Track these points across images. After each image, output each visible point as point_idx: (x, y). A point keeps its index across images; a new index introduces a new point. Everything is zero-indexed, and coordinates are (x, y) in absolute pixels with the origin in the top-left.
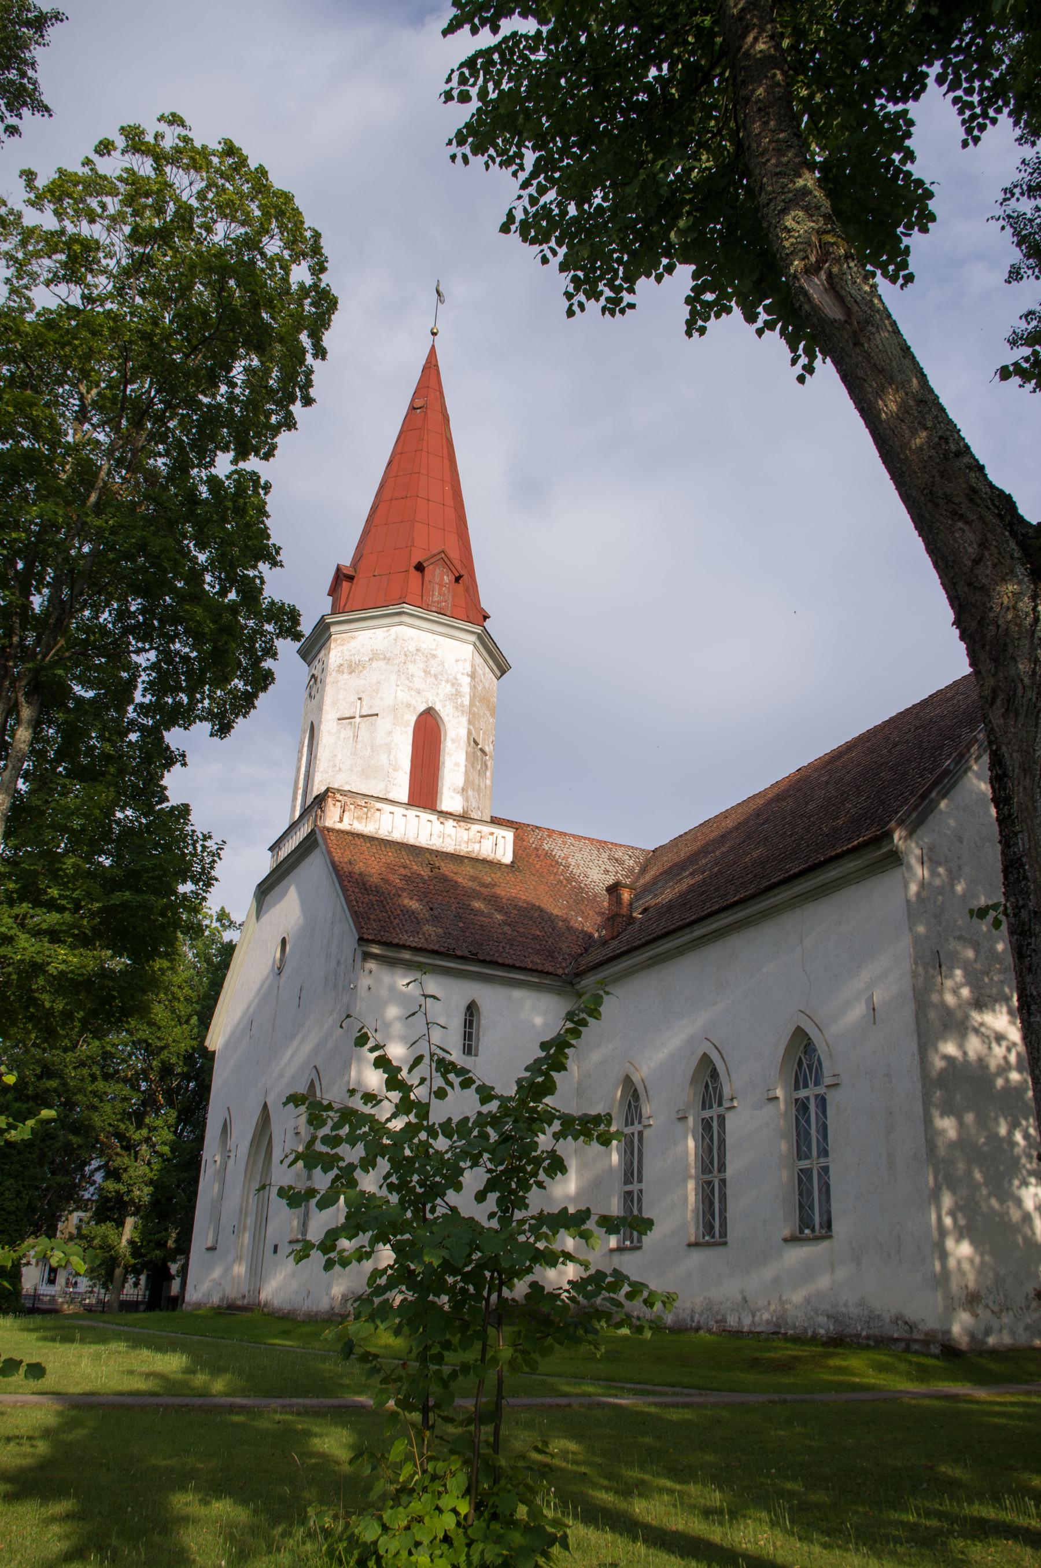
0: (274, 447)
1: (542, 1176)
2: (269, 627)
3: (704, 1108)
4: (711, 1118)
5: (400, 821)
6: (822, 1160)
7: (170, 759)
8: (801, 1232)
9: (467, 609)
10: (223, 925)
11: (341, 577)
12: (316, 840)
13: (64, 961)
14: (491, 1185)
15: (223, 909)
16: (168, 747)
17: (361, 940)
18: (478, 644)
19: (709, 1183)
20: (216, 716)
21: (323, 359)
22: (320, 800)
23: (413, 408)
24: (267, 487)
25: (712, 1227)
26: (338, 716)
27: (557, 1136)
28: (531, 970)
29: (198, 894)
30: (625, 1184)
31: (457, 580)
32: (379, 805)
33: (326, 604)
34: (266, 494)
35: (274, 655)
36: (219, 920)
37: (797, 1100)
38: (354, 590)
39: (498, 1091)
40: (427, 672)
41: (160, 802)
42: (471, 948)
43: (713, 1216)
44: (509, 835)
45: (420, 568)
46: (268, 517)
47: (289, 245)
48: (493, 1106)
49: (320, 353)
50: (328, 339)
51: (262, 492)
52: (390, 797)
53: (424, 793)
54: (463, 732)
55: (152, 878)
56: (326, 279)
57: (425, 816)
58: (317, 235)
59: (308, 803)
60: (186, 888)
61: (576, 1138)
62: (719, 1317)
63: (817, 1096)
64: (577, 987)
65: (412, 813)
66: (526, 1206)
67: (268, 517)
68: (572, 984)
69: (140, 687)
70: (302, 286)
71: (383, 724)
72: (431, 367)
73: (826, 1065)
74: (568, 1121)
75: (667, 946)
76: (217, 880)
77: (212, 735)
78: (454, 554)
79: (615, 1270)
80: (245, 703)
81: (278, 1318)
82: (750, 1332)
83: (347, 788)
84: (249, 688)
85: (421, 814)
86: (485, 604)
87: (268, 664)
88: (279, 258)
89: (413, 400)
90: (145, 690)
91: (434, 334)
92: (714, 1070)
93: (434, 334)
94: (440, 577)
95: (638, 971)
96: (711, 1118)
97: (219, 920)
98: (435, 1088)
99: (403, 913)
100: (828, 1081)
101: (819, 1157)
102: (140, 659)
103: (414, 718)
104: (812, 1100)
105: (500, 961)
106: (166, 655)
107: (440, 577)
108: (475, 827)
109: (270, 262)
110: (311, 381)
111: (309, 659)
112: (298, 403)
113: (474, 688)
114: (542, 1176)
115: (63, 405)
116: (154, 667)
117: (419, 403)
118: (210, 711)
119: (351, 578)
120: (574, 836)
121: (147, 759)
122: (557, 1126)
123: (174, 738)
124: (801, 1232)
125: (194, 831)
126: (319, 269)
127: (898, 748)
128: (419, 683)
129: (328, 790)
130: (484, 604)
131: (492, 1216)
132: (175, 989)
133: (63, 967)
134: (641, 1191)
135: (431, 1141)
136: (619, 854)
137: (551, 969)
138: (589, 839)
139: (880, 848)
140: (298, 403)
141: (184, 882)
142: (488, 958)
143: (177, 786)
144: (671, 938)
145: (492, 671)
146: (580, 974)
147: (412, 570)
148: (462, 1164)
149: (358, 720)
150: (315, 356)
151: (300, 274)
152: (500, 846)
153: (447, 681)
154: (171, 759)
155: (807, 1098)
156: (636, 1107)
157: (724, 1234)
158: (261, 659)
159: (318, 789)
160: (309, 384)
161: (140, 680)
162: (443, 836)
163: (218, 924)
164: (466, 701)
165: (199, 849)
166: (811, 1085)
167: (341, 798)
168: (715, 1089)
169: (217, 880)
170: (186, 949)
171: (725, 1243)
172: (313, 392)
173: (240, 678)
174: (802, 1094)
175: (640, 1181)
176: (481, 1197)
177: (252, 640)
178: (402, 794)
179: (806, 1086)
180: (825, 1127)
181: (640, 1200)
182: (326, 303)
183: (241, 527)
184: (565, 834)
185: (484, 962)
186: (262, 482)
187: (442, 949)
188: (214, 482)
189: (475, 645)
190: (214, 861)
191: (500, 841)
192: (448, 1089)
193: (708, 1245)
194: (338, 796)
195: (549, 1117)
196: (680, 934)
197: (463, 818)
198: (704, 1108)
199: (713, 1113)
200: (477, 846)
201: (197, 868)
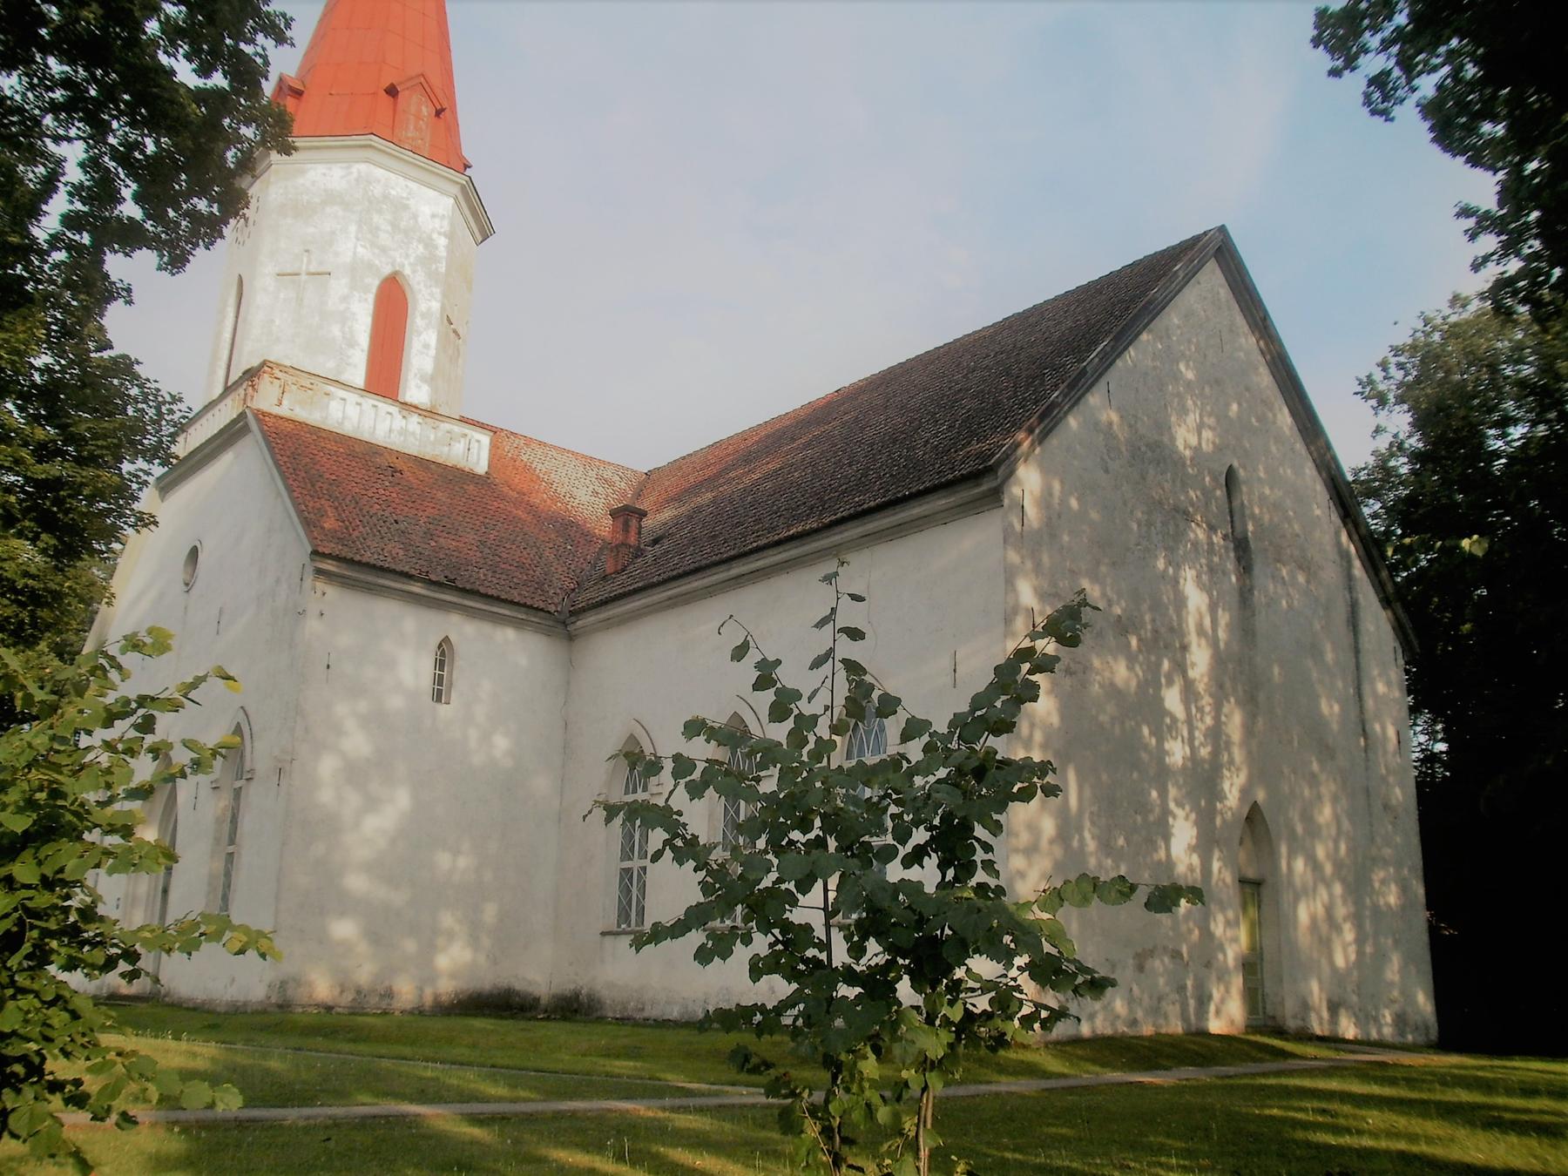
5: (352, 412)
9: (445, 152)
17: (315, 553)
18: (461, 198)
20: (165, 243)
22: (251, 375)
25: (628, 916)
26: (277, 270)
28: (518, 604)
29: (137, 477)
31: (438, 113)
40: (395, 226)
42: (447, 573)
44: (485, 439)
45: (392, 91)
52: (342, 379)
53: (384, 377)
54: (435, 306)
57: (385, 407)
59: (233, 378)
65: (369, 401)
68: (564, 624)
71: (338, 286)
75: (695, 584)
78: (435, 81)
80: (208, 229)
81: (188, 1009)
83: (288, 363)
85: (380, 405)
86: (468, 153)
95: (650, 613)
105: (482, 590)
107: (416, 106)
108: (446, 426)
113: (450, 250)
119: (298, 94)
120: (555, 447)
123: (116, 265)
125: (158, 390)
127: (978, 374)
128: (384, 239)
129: (264, 363)
136: (608, 474)
137: (542, 605)
139: (978, 485)
142: (468, 587)
143: (121, 328)
144: (699, 575)
146: (576, 613)
149: (304, 277)
152: (473, 453)
154: (111, 292)
167: (280, 375)
178: (358, 377)
185: (465, 592)
187: (413, 572)
189: (456, 199)
191: (474, 445)
194: (277, 372)
196: (714, 570)
197: (430, 413)
200: (446, 449)
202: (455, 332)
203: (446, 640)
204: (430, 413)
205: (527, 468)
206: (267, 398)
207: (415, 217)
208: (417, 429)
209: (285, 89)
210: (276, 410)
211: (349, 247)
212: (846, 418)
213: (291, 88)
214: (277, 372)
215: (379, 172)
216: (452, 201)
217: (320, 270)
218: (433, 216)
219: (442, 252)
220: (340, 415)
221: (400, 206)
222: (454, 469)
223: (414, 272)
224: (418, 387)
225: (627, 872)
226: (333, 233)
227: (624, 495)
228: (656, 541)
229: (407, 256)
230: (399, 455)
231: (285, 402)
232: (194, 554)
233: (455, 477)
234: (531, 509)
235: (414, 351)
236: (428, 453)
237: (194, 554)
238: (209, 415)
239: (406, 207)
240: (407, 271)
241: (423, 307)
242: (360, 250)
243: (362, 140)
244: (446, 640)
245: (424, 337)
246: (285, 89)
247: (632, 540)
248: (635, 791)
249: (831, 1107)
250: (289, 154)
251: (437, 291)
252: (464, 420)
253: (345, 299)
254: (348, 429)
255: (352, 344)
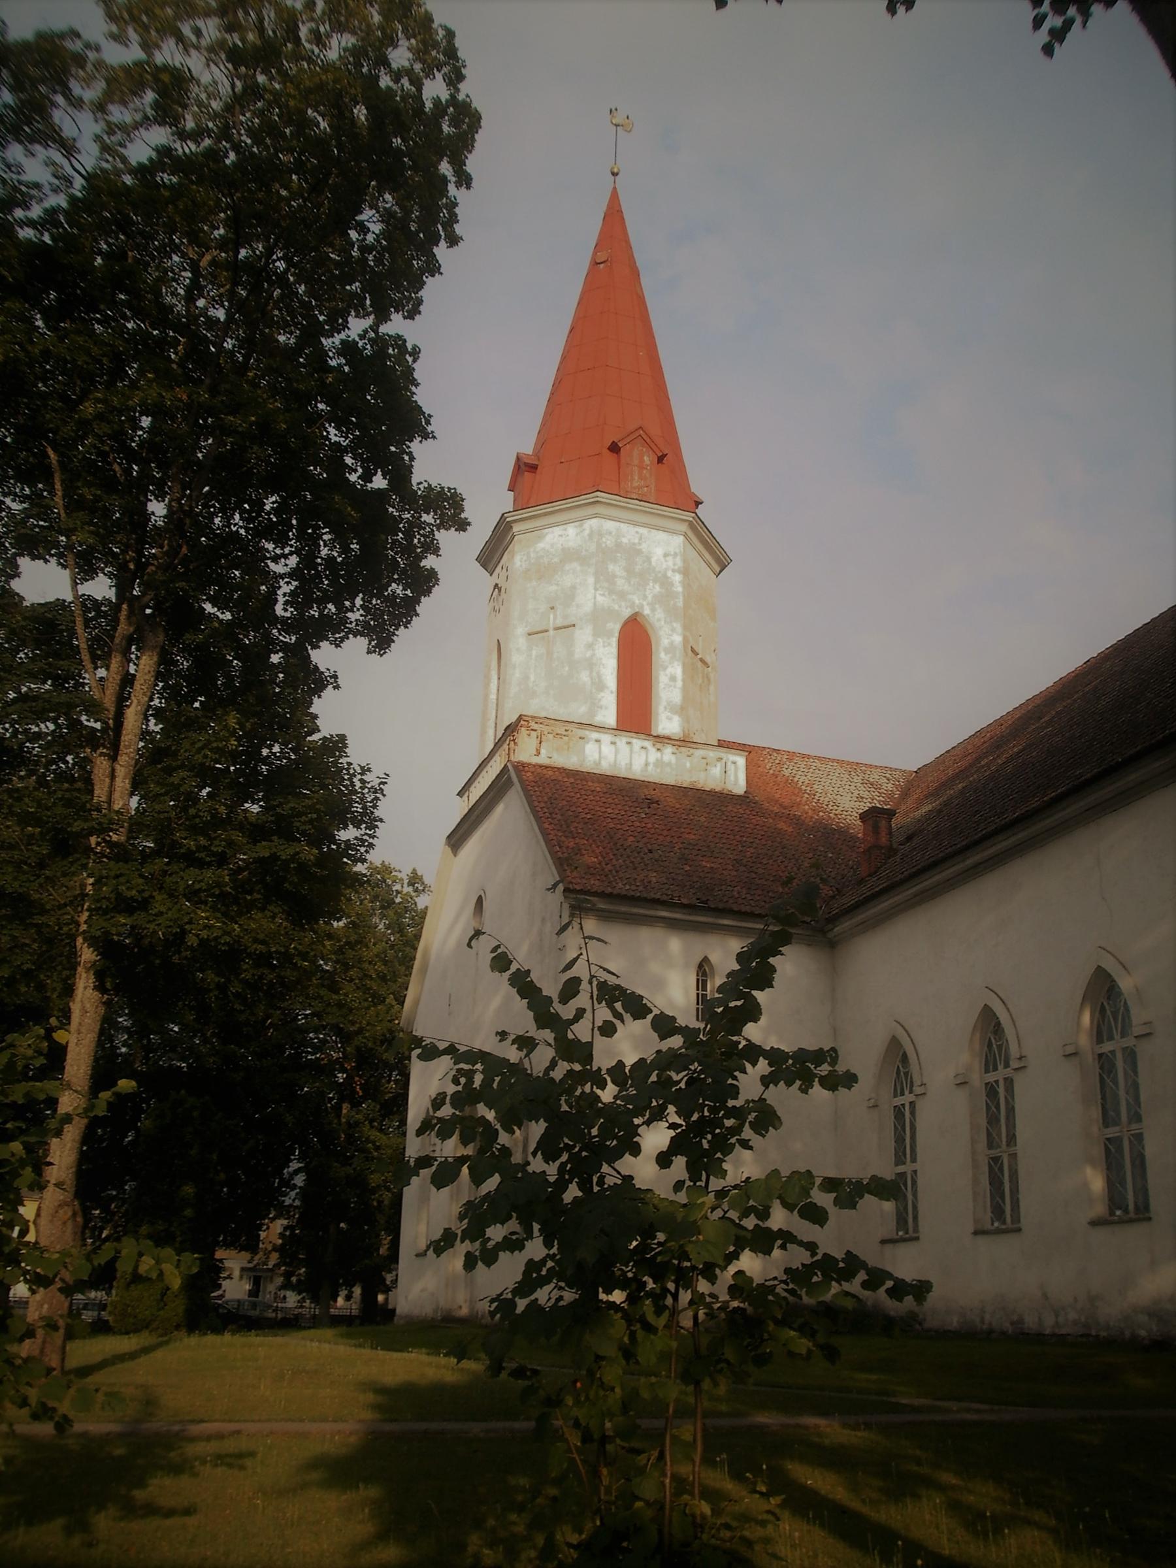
0: (420, 302)
1: (747, 1133)
2: (427, 518)
3: (987, 1071)
4: (997, 1082)
5: (607, 750)
6: (1134, 1126)
7: (319, 682)
8: (1112, 1213)
9: (673, 493)
10: (416, 890)
11: (524, 468)
12: (509, 778)
13: (206, 927)
14: (676, 1146)
15: (414, 872)
16: (316, 667)
18: (690, 534)
19: (996, 1160)
21: (468, 187)
23: (595, 263)
24: (416, 353)
25: (1003, 1212)
27: (766, 1081)
29: (363, 841)
30: (897, 1165)
31: (660, 460)
32: (581, 733)
33: (506, 501)
34: (414, 361)
35: (436, 551)
36: (411, 884)
37: (1100, 1056)
38: (536, 481)
39: (681, 1021)
40: (629, 571)
41: (311, 733)
43: (1003, 1197)
44: (741, 761)
45: (614, 448)
46: (417, 385)
47: (420, 54)
48: (676, 1041)
49: (465, 180)
50: (473, 163)
51: (410, 359)
53: (635, 715)
54: (678, 639)
55: (304, 823)
56: (465, 88)
57: (637, 743)
58: (450, 34)
60: (348, 834)
61: (789, 1084)
62: (1015, 1318)
63: (1124, 1049)
64: (830, 935)
65: (622, 740)
66: (724, 1173)
67: (417, 385)
68: (823, 932)
69: (281, 600)
70: (437, 102)
71: (583, 635)
72: (614, 216)
73: (1134, 1011)
74: (775, 1056)
76: (381, 820)
77: (369, 652)
79: (848, 1253)
80: (405, 611)
82: (1053, 1335)
83: (543, 714)
84: (409, 592)
86: (697, 485)
87: (429, 562)
88: (409, 72)
89: (595, 253)
90: (286, 603)
91: (614, 174)
92: (998, 1024)
93: (614, 174)
94: (640, 458)
96: (997, 1082)
97: (411, 884)
98: (599, 1023)
99: (611, 850)
100: (1137, 1031)
101: (1130, 1123)
102: (277, 568)
103: (618, 627)
104: (1119, 1055)
106: (308, 559)
107: (640, 458)
108: (699, 753)
109: (397, 76)
110: (456, 216)
111: (490, 567)
112: (443, 244)
113: (686, 585)
114: (747, 1133)
115: (176, 281)
116: (293, 574)
117: (601, 257)
118: (366, 625)
119: (533, 468)
121: (291, 682)
122: (763, 1064)
123: (323, 656)
124: (1112, 1213)
125: (349, 764)
126: (455, 78)
128: (621, 583)
129: (520, 718)
130: (694, 489)
131: (678, 1186)
132: (366, 966)
133: (204, 934)
134: (915, 1172)
135: (599, 1092)
136: (874, 777)
138: (838, 761)
140: (443, 244)
141: (345, 827)
142: (721, 906)
143: (329, 714)
145: (709, 565)
146: (833, 920)
147: (606, 452)
148: (636, 1121)
149: (552, 632)
150: (458, 185)
151: (435, 89)
152: (731, 775)
153: (655, 581)
155: (1113, 1052)
156: (906, 1074)
157: (1016, 1218)
158: (420, 558)
159: (509, 718)
160: (453, 219)
161: (280, 592)
162: (659, 763)
163: (410, 889)
164: (680, 603)
165: (358, 785)
166: (1117, 1036)
167: (536, 727)
168: (1000, 1047)
169: (381, 820)
170: (376, 920)
171: (1019, 1230)
172: (458, 229)
173: (398, 581)
174: (1107, 1047)
175: (914, 1160)
176: (664, 1160)
177: (409, 535)
178: (609, 716)
179: (1111, 1038)
180: (1136, 1086)
181: (914, 1183)
182: (467, 118)
183: (384, 403)
184: (809, 757)
186: (409, 348)
187: (665, 898)
188: (348, 349)
189: (685, 535)
190: (377, 799)
191: (731, 767)
192: (617, 1022)
193: (998, 1232)
194: (533, 725)
195: (753, 1052)
197: (683, 742)
198: (987, 1071)
199: (1000, 1074)
201: (358, 807)
202: (702, 660)
203: (706, 960)
204: (683, 742)
205: (789, 782)
206: (526, 751)
207: (648, 559)
208: (673, 759)
209: (522, 466)
210: (535, 760)
211: (590, 597)
212: (1087, 689)
213: (526, 464)
214: (533, 725)
215: (610, 525)
216: (682, 538)
217: (566, 624)
218: (666, 555)
219: (679, 589)
220: (597, 756)
221: (633, 552)
222: (712, 793)
223: (653, 610)
224: (670, 719)
225: (996, 1160)
226: (573, 588)
227: (890, 796)
228: (909, 838)
229: (645, 597)
230: (656, 786)
231: (543, 751)
232: (480, 901)
233: (718, 800)
234: (797, 821)
235: (661, 685)
236: (686, 780)
237: (480, 901)
238: (484, 773)
239: (639, 552)
240: (647, 611)
241: (665, 642)
242: (600, 599)
243: (589, 498)
244: (706, 960)
245: (670, 670)
246: (522, 466)
247: (884, 840)
248: (902, 1094)
249: (575, 1542)
250: (465, 530)
251: (678, 626)
252: (722, 744)
253: (590, 646)
254: (605, 768)
255: (601, 686)
